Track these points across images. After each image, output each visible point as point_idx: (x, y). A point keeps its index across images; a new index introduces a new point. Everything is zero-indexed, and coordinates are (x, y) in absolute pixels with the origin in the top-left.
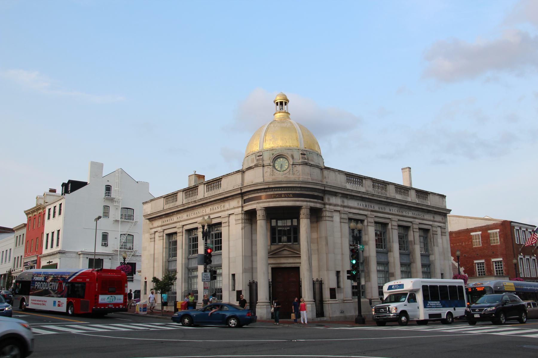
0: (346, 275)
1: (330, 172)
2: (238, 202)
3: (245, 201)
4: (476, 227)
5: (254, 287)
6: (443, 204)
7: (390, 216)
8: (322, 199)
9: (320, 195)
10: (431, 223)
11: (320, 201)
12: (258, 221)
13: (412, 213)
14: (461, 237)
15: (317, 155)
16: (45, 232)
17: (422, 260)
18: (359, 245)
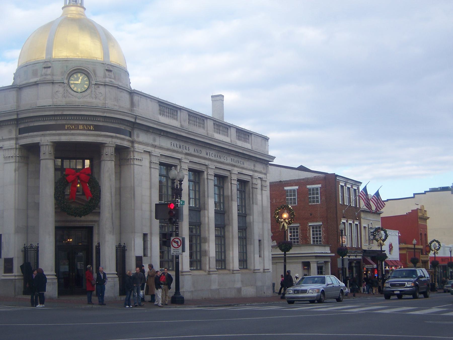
3: (21, 131)
4: (292, 180)
6: (265, 148)
7: (207, 162)
10: (251, 173)
12: (42, 161)
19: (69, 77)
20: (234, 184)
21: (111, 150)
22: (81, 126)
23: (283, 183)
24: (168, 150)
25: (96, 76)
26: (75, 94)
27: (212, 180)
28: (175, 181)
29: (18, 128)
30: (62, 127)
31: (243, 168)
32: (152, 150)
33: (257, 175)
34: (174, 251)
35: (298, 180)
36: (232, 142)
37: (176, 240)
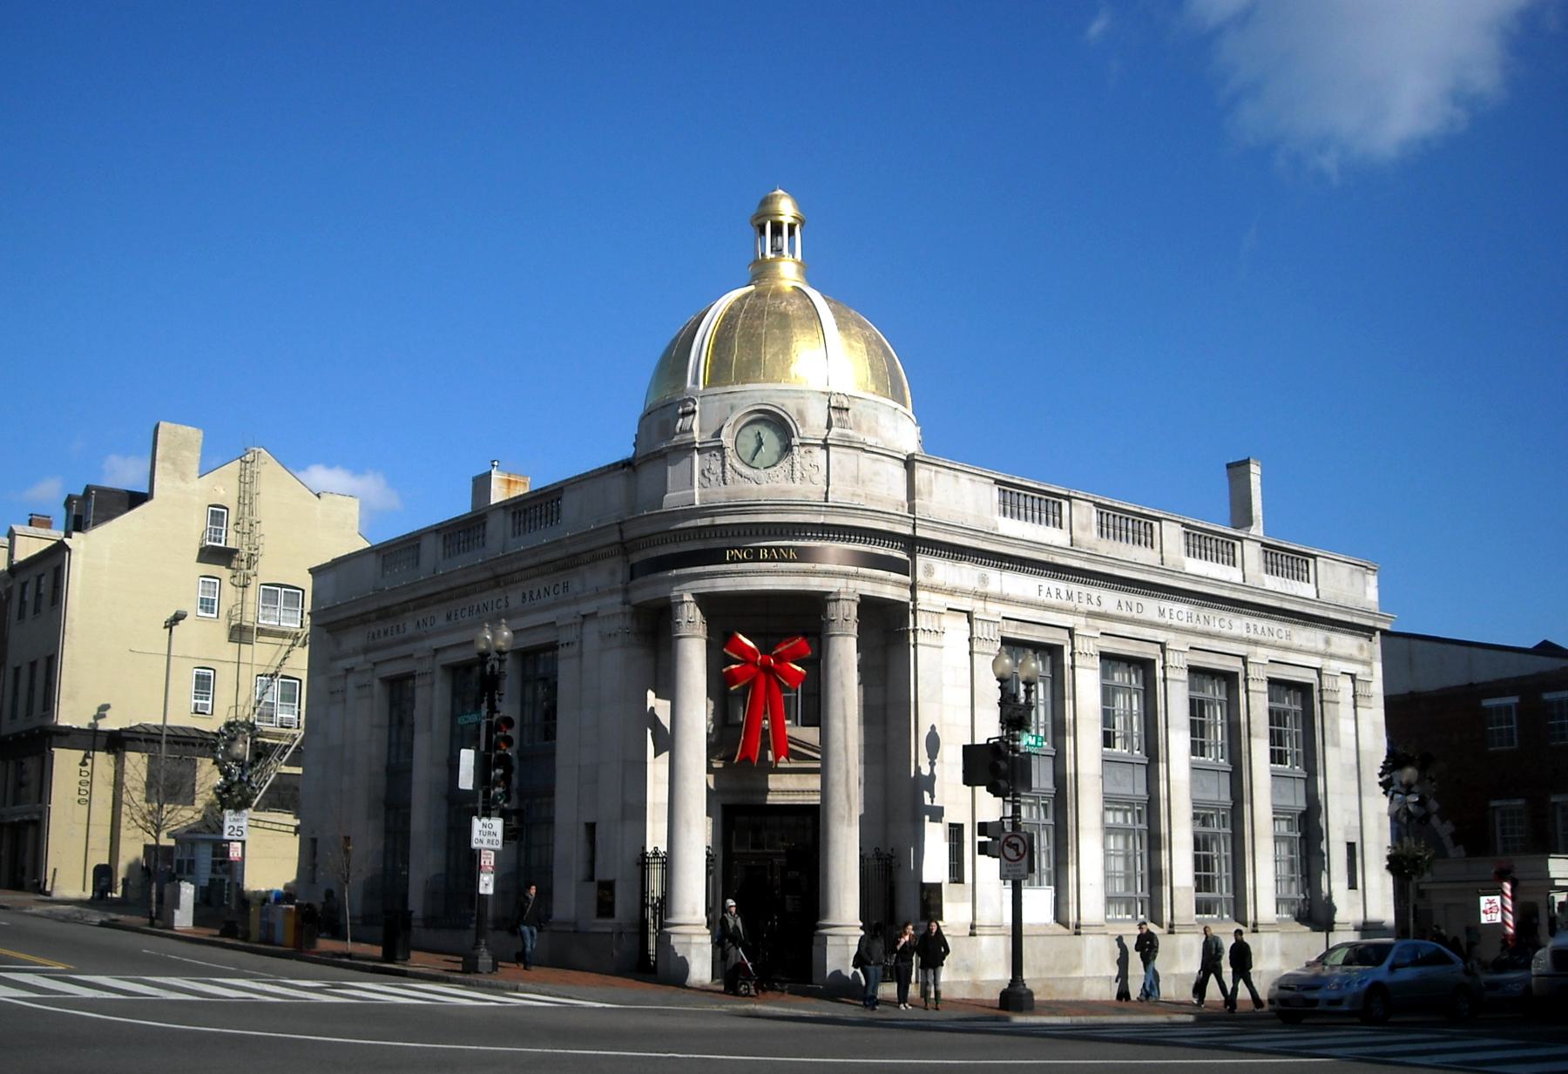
1: (936, 472)
2: (613, 573)
3: (634, 572)
4: (1500, 681)
7: (1161, 636)
10: (1316, 662)
13: (1245, 626)
15: (895, 414)
16: (13, 660)
20: (1255, 691)
21: (843, 609)
22: (764, 551)
24: (1027, 604)
25: (803, 426)
31: (1287, 649)
34: (1008, 871)
35: (1516, 679)
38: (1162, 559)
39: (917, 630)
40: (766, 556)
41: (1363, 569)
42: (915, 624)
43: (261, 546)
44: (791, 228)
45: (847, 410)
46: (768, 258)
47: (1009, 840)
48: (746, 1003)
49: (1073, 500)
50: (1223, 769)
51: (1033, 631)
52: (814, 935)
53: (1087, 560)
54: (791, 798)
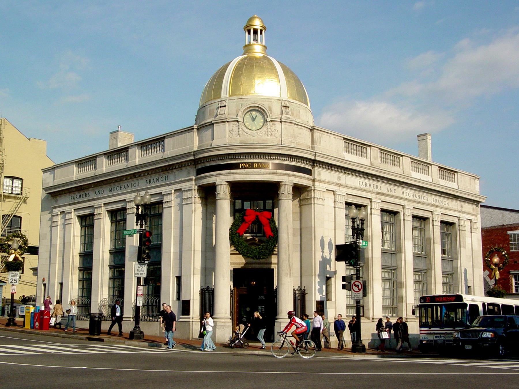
0: (340, 283)
1: (322, 134)
3: (200, 172)
5: (208, 296)
7: (403, 202)
8: (308, 172)
9: (309, 167)
10: (457, 214)
11: (307, 176)
14: (494, 237)
17: (443, 267)
18: (361, 241)
19: (243, 116)
21: (287, 189)
23: (507, 227)
24: (355, 188)
25: (271, 113)
26: (249, 131)
27: (409, 221)
28: (355, 220)
29: (196, 168)
30: (235, 166)
31: (447, 209)
32: (336, 188)
33: (464, 216)
34: (355, 296)
36: (404, 173)
37: (357, 283)
38: (403, 172)
39: (315, 198)
40: (257, 166)
41: (475, 178)
42: (314, 196)
43: (5, 160)
44: (261, 31)
45: (288, 107)
46: (252, 43)
47: (355, 283)
48: (241, 351)
49: (372, 147)
50: (424, 256)
51: (356, 199)
52: (274, 322)
53: (378, 171)
54: (262, 266)
